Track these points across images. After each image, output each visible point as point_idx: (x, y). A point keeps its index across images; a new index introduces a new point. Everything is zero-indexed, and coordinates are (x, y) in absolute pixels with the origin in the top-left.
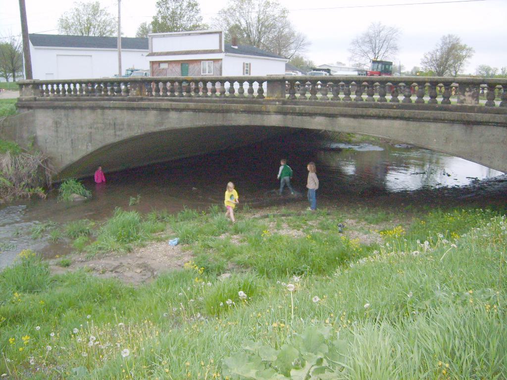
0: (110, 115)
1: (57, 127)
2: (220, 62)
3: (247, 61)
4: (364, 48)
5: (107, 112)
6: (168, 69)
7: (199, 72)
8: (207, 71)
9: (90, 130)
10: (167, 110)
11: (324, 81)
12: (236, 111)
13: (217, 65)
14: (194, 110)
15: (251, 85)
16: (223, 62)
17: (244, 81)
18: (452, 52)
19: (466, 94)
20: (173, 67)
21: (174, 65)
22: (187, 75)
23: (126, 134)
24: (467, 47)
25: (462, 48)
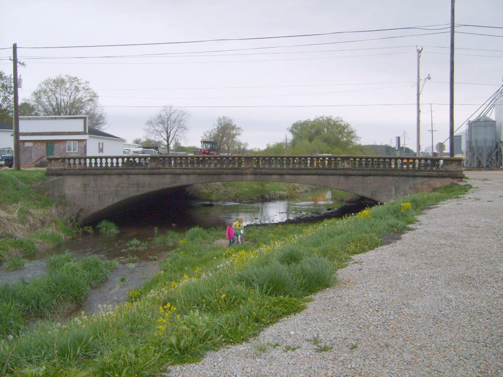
0: (134, 178)
1: (85, 187)
2: (84, 142)
3: (101, 141)
4: (157, 128)
5: (131, 176)
6: (33, 147)
7: (65, 150)
8: (73, 150)
9: (116, 189)
10: (180, 174)
11: (246, 158)
12: (227, 174)
13: (82, 145)
14: (199, 174)
15: (106, 160)
16: (87, 141)
17: (76, 159)
18: (226, 130)
19: (345, 162)
20: (39, 146)
21: (39, 144)
22: (53, 155)
23: (146, 190)
24: (237, 127)
25: (233, 128)
